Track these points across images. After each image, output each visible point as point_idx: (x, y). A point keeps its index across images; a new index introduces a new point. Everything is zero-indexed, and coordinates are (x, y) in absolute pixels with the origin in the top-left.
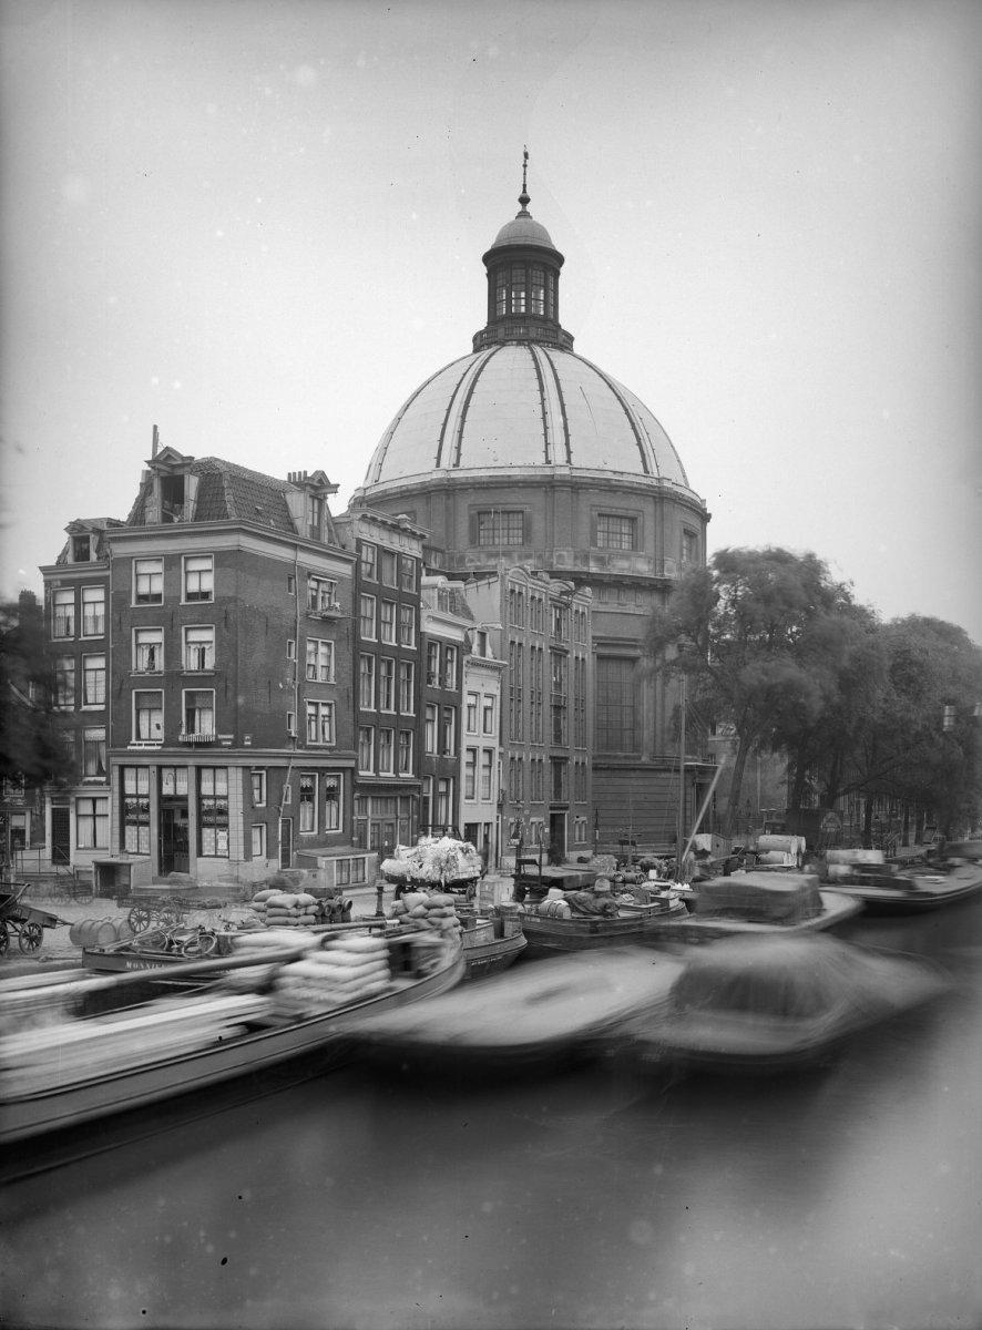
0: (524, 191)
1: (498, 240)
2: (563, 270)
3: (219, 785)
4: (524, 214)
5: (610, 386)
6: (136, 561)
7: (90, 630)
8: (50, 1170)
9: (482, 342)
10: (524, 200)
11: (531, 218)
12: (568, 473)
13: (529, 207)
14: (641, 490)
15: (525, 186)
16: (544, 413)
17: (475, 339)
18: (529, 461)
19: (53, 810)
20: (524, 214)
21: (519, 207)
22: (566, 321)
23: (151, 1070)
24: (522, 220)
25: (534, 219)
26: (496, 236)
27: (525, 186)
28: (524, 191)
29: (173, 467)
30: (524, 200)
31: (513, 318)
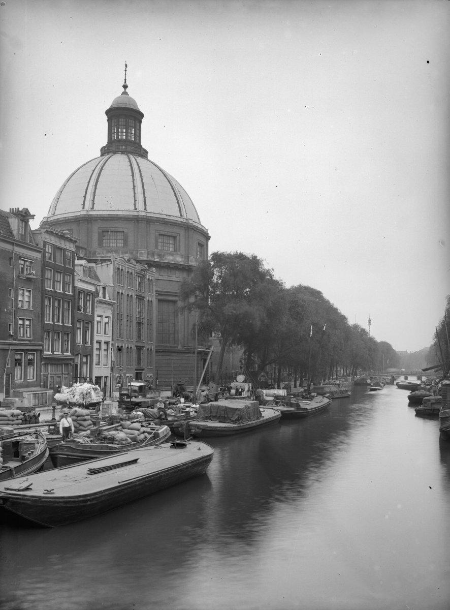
0: (125, 82)
1: (113, 104)
2: (143, 120)
4: (125, 93)
10: (125, 87)
13: (127, 90)
14: (178, 224)
15: (125, 80)
16: (134, 186)
17: (101, 150)
18: (127, 208)
20: (125, 93)
21: (123, 90)
22: (145, 144)
27: (125, 80)
28: (125, 82)
30: (125, 87)
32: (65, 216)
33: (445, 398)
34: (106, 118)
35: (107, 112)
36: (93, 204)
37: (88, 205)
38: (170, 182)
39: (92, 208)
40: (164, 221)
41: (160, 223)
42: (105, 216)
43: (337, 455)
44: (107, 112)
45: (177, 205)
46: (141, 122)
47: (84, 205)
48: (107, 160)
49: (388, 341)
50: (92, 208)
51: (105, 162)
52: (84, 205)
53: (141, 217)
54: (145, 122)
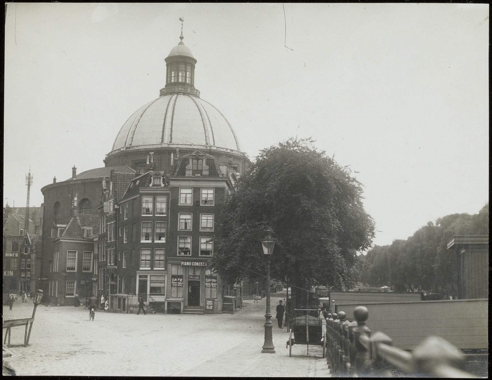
0: (182, 34)
2: (196, 65)
3: (179, 272)
4: (181, 43)
5: (222, 115)
6: (181, 188)
7: (158, 211)
8: (478, 301)
9: (163, 93)
10: (182, 38)
11: (184, 45)
12: (167, 146)
13: (183, 41)
14: (238, 157)
15: (182, 32)
16: (204, 125)
17: (161, 91)
18: (200, 143)
19: (139, 280)
21: (180, 40)
22: (196, 86)
23: (427, 303)
24: (180, 46)
25: (185, 45)
26: (170, 51)
27: (182, 32)
28: (182, 34)
29: (199, 156)
30: (182, 38)
31: (177, 84)
32: (146, 147)
33: (72, 268)
34: (165, 63)
35: (166, 60)
36: (171, 138)
37: (167, 139)
38: (226, 121)
39: (171, 142)
40: (230, 155)
41: (226, 156)
42: (184, 149)
43: (466, 374)
44: (166, 60)
45: (212, 127)
46: (194, 67)
47: (163, 138)
48: (175, 101)
49: (40, 190)
50: (171, 142)
51: (175, 103)
52: (163, 138)
53: (213, 151)
54: (198, 67)
